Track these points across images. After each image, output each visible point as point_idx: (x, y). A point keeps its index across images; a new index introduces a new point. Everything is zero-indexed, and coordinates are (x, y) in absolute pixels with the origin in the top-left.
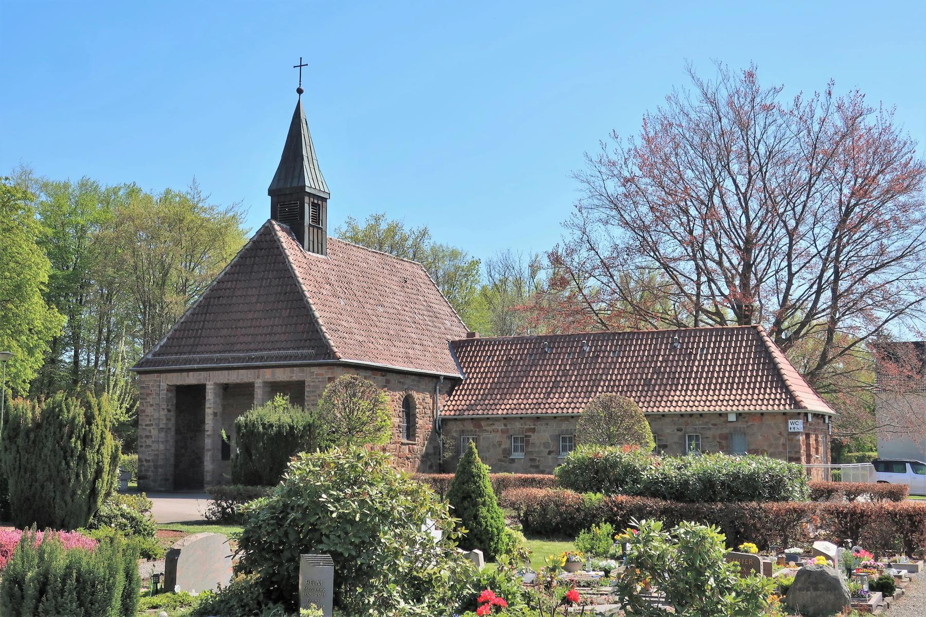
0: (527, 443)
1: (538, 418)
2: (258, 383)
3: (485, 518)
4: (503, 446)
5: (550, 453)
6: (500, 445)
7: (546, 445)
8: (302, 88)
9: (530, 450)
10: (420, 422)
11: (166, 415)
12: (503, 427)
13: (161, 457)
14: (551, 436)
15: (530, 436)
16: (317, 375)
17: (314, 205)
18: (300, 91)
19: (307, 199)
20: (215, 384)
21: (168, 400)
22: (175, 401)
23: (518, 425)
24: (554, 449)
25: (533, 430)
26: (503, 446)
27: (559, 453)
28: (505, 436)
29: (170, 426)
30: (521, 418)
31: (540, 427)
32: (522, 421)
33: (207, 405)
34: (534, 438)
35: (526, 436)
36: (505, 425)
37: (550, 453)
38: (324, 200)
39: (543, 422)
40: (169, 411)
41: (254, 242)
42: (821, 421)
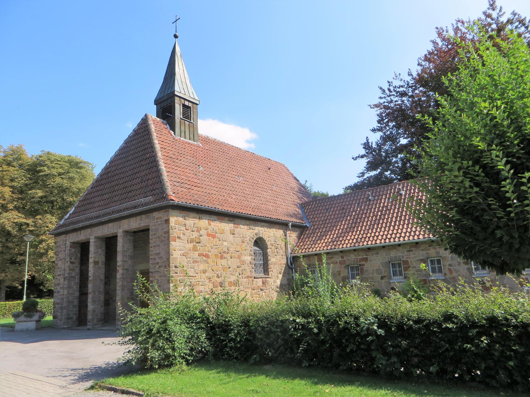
0: (362, 270)
1: (369, 249)
2: (120, 234)
3: (395, 105)
4: (342, 275)
5: (382, 278)
6: (339, 274)
7: (378, 271)
8: (177, 34)
9: (364, 276)
10: (272, 260)
11: (69, 266)
12: (341, 259)
13: (65, 300)
14: (381, 263)
15: (364, 265)
16: (157, 219)
17: (184, 106)
18: (176, 36)
19: (177, 100)
20: (95, 237)
21: (71, 255)
22: (79, 255)
23: (352, 257)
24: (386, 274)
25: (366, 260)
26: (342, 275)
27: (390, 278)
28: (343, 266)
29: (73, 274)
30: (355, 250)
31: (371, 257)
32: (356, 253)
33: (90, 256)
34: (367, 266)
35: (360, 265)
36: (342, 257)
37: (382, 278)
38: (197, 104)
39: (374, 252)
40: (72, 263)
41: (135, 131)
42: (291, 270)
